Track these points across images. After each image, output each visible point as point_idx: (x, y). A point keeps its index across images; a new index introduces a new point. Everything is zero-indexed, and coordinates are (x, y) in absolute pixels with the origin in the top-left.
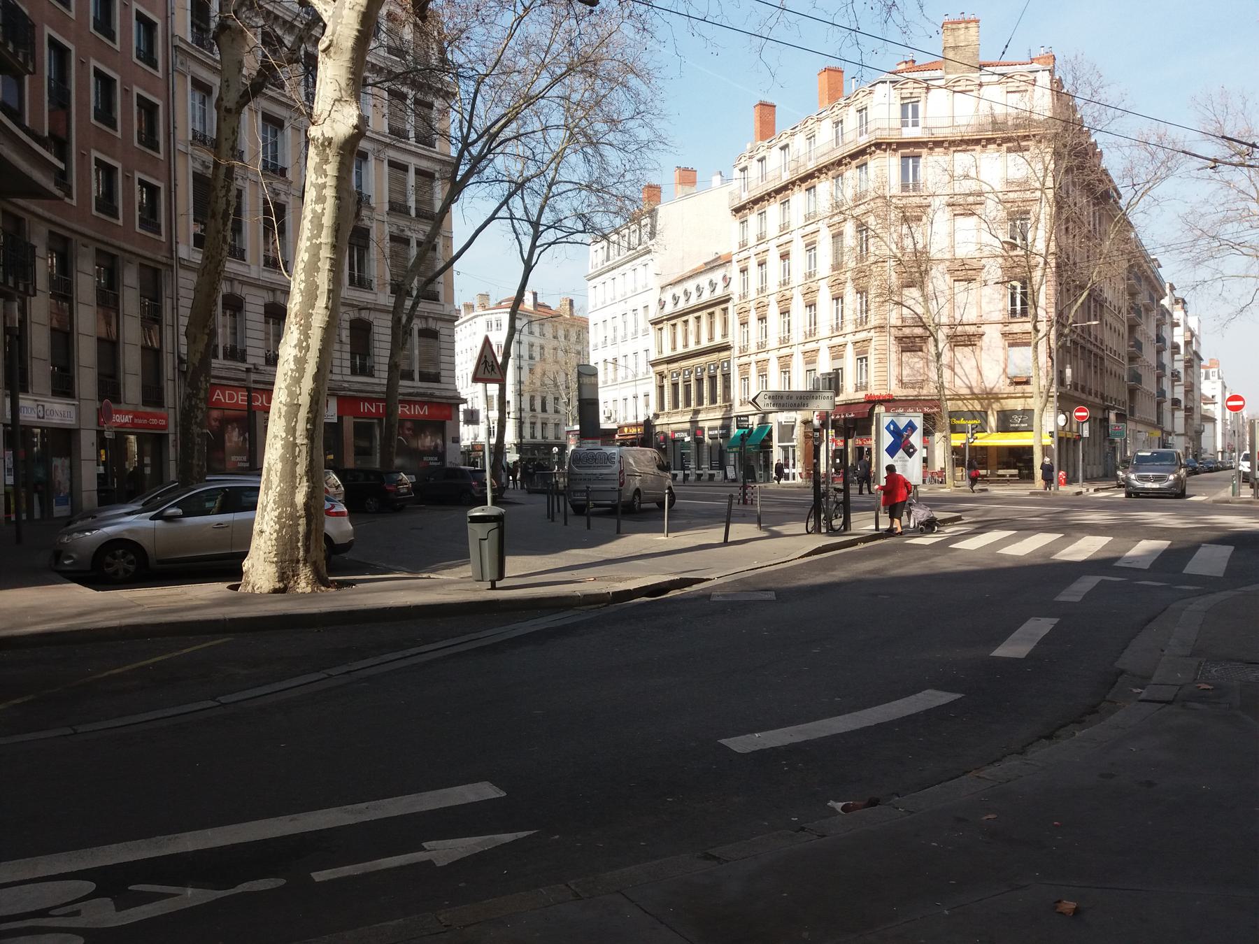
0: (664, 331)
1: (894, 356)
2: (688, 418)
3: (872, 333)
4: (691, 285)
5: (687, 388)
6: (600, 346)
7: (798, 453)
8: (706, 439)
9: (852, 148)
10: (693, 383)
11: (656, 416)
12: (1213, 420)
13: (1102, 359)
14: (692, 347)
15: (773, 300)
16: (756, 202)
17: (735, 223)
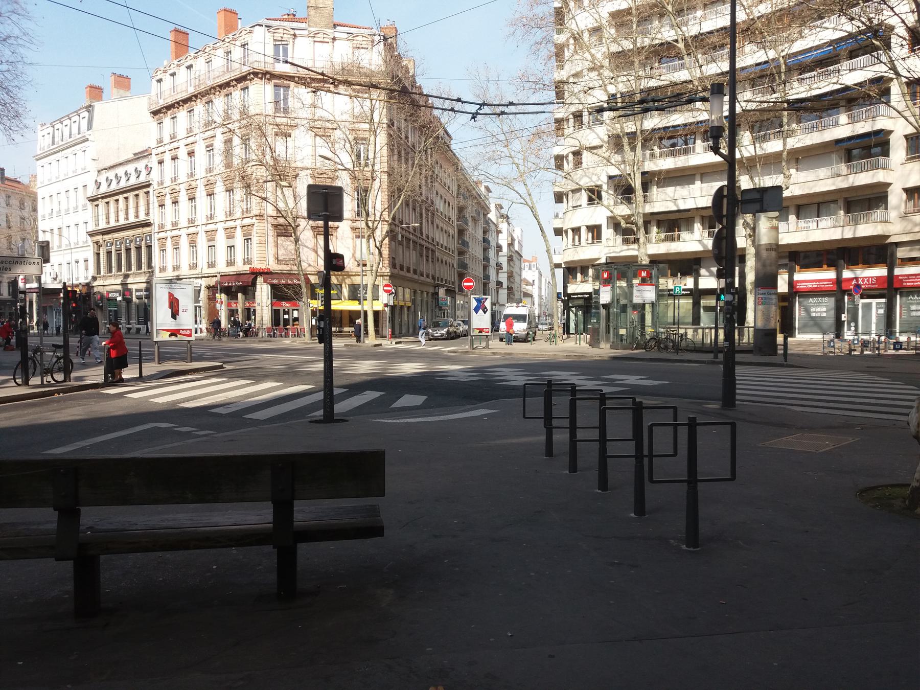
0: (100, 206)
1: (271, 239)
2: (119, 281)
3: (254, 220)
4: (120, 171)
5: (119, 256)
6: (47, 217)
7: (203, 312)
8: (134, 299)
9: (236, 74)
10: (123, 252)
11: (94, 279)
12: (531, 296)
13: (433, 251)
14: (122, 222)
15: (183, 188)
16: (169, 107)
17: (152, 123)
